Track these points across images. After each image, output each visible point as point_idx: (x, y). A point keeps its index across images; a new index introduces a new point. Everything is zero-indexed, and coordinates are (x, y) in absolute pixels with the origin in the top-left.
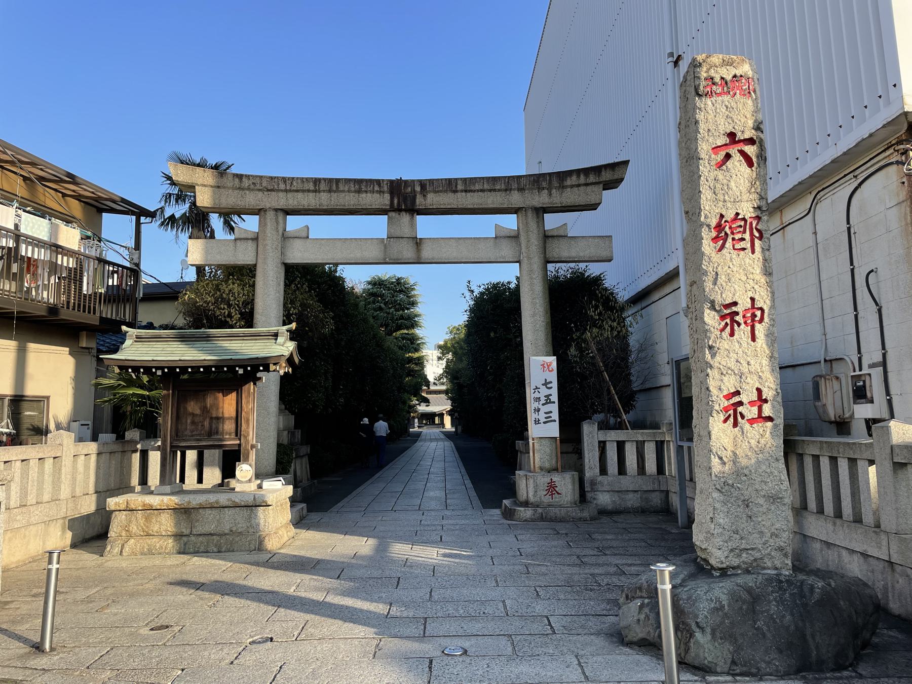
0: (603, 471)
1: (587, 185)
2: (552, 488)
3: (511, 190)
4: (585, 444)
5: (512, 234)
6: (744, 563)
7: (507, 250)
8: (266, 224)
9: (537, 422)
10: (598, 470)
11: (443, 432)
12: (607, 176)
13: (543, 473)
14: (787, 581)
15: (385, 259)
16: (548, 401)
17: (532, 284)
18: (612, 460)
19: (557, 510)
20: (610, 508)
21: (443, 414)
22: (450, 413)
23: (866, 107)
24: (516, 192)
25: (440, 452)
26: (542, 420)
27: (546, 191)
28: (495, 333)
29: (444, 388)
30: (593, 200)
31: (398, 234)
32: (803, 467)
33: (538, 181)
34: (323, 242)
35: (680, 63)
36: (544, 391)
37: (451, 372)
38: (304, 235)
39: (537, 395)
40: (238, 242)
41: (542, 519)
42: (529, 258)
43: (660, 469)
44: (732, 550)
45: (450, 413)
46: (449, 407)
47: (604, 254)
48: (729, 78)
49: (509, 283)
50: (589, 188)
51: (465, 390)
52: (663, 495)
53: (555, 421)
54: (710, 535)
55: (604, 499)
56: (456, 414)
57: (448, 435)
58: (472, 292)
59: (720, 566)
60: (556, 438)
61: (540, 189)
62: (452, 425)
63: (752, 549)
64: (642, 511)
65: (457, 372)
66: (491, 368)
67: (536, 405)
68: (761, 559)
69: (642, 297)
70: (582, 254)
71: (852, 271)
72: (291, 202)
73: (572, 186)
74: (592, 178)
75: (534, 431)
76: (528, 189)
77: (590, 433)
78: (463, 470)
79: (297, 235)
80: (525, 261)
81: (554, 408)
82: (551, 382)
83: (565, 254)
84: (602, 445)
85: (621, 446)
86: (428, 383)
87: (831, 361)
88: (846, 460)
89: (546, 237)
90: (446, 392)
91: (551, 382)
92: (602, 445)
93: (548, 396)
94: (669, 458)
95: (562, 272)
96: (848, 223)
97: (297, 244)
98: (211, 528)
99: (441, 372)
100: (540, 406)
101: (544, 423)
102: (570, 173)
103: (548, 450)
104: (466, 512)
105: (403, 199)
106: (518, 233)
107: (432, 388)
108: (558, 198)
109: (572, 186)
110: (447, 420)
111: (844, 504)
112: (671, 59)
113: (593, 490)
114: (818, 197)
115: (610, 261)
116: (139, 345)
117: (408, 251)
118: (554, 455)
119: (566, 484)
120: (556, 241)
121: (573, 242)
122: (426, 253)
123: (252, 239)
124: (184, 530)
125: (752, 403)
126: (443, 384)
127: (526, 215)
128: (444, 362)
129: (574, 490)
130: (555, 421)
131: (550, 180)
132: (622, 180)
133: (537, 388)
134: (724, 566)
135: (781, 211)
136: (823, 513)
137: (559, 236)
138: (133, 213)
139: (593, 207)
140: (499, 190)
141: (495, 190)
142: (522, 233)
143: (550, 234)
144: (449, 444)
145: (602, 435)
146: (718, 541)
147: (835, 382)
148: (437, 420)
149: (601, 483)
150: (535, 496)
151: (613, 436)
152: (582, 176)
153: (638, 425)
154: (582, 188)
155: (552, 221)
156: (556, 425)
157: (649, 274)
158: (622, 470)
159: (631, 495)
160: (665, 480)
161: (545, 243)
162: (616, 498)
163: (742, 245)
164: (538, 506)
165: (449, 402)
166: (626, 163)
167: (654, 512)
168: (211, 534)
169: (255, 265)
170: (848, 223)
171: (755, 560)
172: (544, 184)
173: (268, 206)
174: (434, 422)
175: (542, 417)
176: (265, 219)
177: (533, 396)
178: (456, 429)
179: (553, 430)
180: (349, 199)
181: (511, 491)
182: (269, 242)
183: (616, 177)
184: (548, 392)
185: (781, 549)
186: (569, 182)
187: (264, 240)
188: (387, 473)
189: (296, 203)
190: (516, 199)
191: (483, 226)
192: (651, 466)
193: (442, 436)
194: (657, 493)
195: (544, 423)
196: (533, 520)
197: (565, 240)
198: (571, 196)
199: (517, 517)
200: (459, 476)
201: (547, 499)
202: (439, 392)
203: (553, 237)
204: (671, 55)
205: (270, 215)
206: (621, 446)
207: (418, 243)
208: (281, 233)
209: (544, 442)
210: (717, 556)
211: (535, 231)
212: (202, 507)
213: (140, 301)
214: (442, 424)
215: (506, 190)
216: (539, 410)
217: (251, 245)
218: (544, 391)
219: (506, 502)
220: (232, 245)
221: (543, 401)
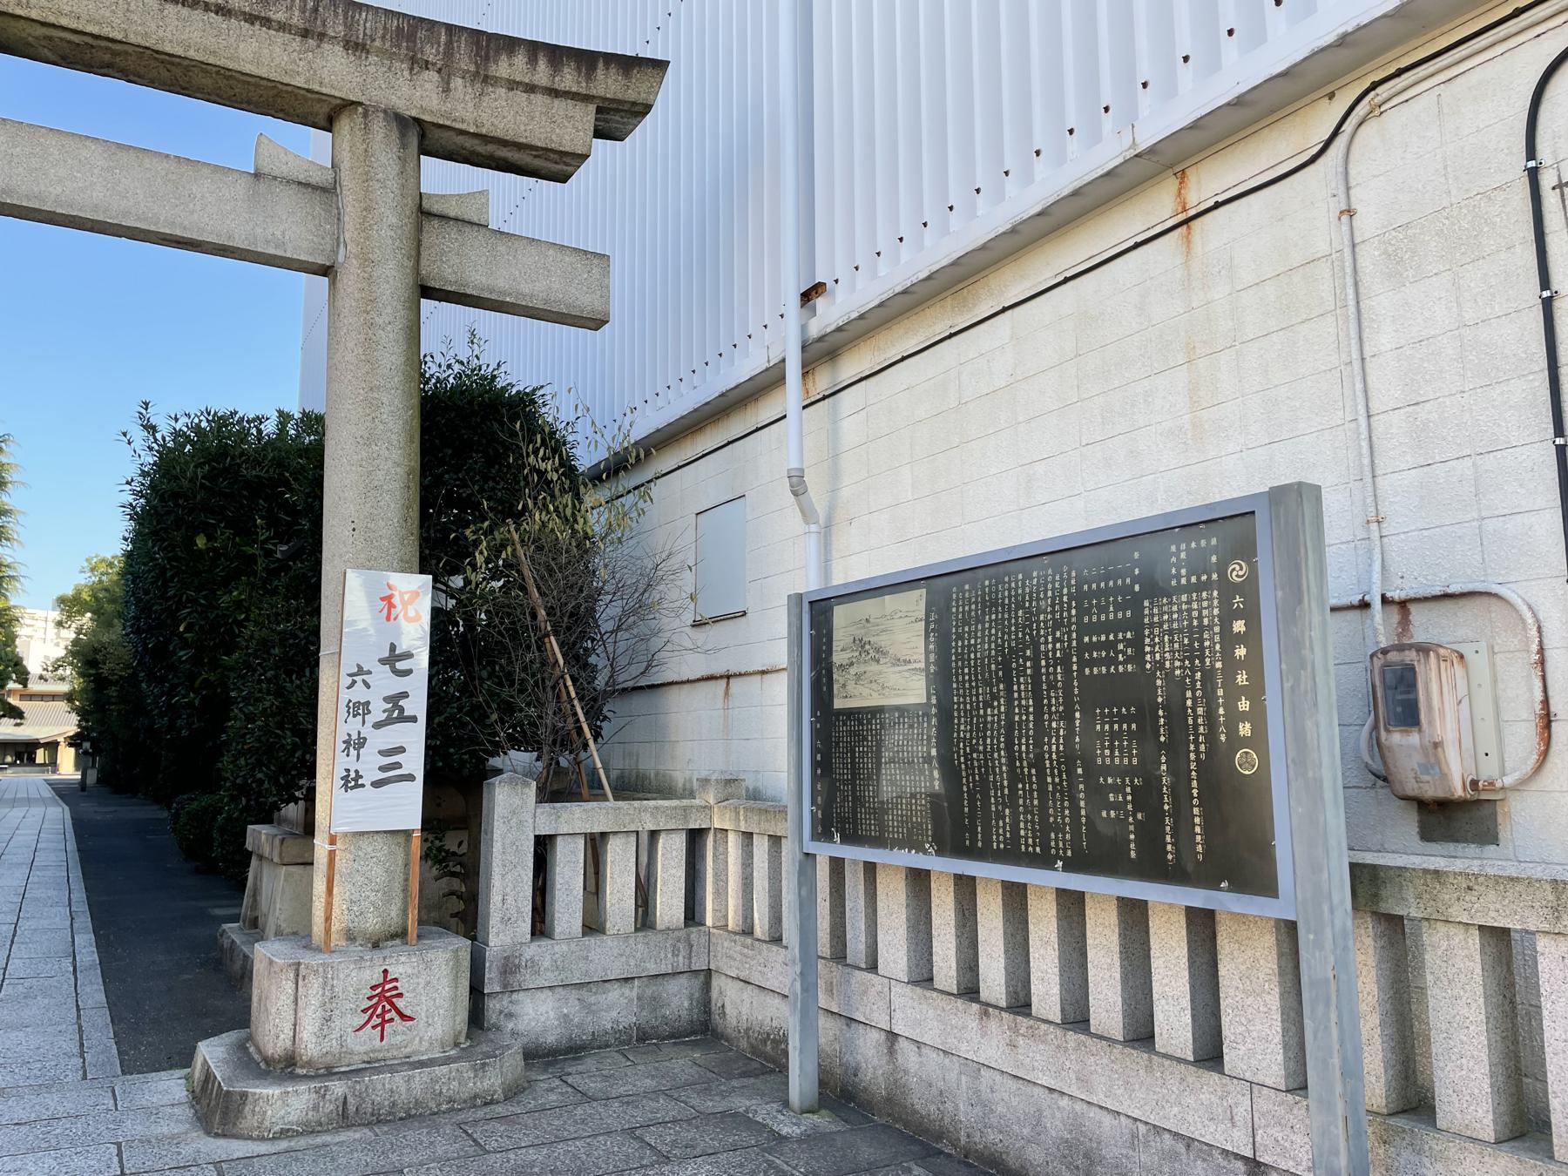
0: (541, 924)
1: (554, 93)
2: (384, 1003)
3: (322, 36)
4: (497, 847)
5: (316, 178)
9: (352, 781)
10: (526, 926)
11: (51, 783)
12: (608, 84)
13: (356, 948)
16: (396, 714)
18: (569, 890)
19: (398, 1081)
20: (551, 1039)
21: (58, 744)
22: (74, 742)
23: (951, 208)
24: (339, 49)
25: (26, 836)
26: (370, 774)
27: (432, 75)
28: (210, 538)
29: (64, 688)
32: (1297, 952)
33: (411, 37)
36: (384, 683)
37: (87, 657)
39: (359, 694)
41: (345, 1118)
42: (366, 261)
43: (692, 913)
45: (74, 742)
46: (71, 727)
47: (585, 302)
49: (260, 420)
50: (560, 105)
51: (113, 692)
52: (697, 983)
53: (410, 778)
55: (536, 1014)
56: (87, 745)
57: (63, 792)
58: (151, 429)
60: (407, 834)
61: (417, 63)
62: (77, 766)
64: (643, 1039)
65: (96, 651)
66: (189, 629)
67: (354, 726)
69: (617, 466)
70: (525, 288)
71: (1548, 305)
73: (513, 85)
74: (568, 79)
75: (337, 809)
76: (381, 52)
77: (513, 810)
78: (79, 894)
80: (350, 279)
81: (413, 740)
82: (408, 655)
84: (543, 847)
85: (596, 844)
86: (23, 677)
87: (1403, 605)
88: (1475, 939)
89: (424, 214)
90: (69, 697)
91: (408, 655)
92: (543, 847)
93: (395, 700)
94: (721, 877)
95: (434, 369)
96: (1531, 153)
99: (62, 653)
100: (367, 731)
101: (377, 784)
102: (511, 44)
103: (378, 874)
104: (52, 1101)
107: (35, 686)
109: (513, 85)
110: (67, 756)
111: (680, 873)
113: (508, 989)
114: (1361, 110)
118: (397, 886)
119: (431, 979)
120: (452, 231)
121: (502, 249)
126: (62, 679)
128: (69, 634)
129: (454, 999)
130: (410, 778)
131: (449, 43)
132: (646, 109)
133: (360, 671)
135: (1182, 175)
136: (1085, 1022)
140: (282, 27)
141: (267, 22)
143: (436, 208)
144: (59, 814)
145: (549, 819)
147: (1458, 669)
148: (40, 757)
149: (533, 964)
150: (322, 1035)
151: (575, 819)
152: (542, 64)
153: (631, 787)
154: (539, 99)
156: (414, 793)
157: (660, 401)
158: (593, 925)
159: (615, 994)
160: (703, 940)
161: (419, 229)
162: (572, 1007)
164: (330, 1073)
165: (75, 718)
166: (661, 65)
167: (672, 1036)
170: (1531, 153)
172: (430, 53)
174: (32, 761)
175: (369, 764)
177: (345, 695)
178: (84, 775)
179: (405, 807)
181: (225, 996)
183: (631, 95)
184: (398, 685)
186: (503, 68)
192: (669, 903)
193: (47, 793)
194: (683, 980)
195: (377, 784)
196: (309, 1130)
199: (249, 1121)
200: (60, 918)
201: (365, 1043)
202: (54, 697)
203: (444, 218)
206: (596, 844)
209: (367, 846)
211: (393, 184)
213: (25, 686)
214: (53, 763)
215: (305, 34)
216: (361, 743)
218: (384, 683)
221: (378, 714)
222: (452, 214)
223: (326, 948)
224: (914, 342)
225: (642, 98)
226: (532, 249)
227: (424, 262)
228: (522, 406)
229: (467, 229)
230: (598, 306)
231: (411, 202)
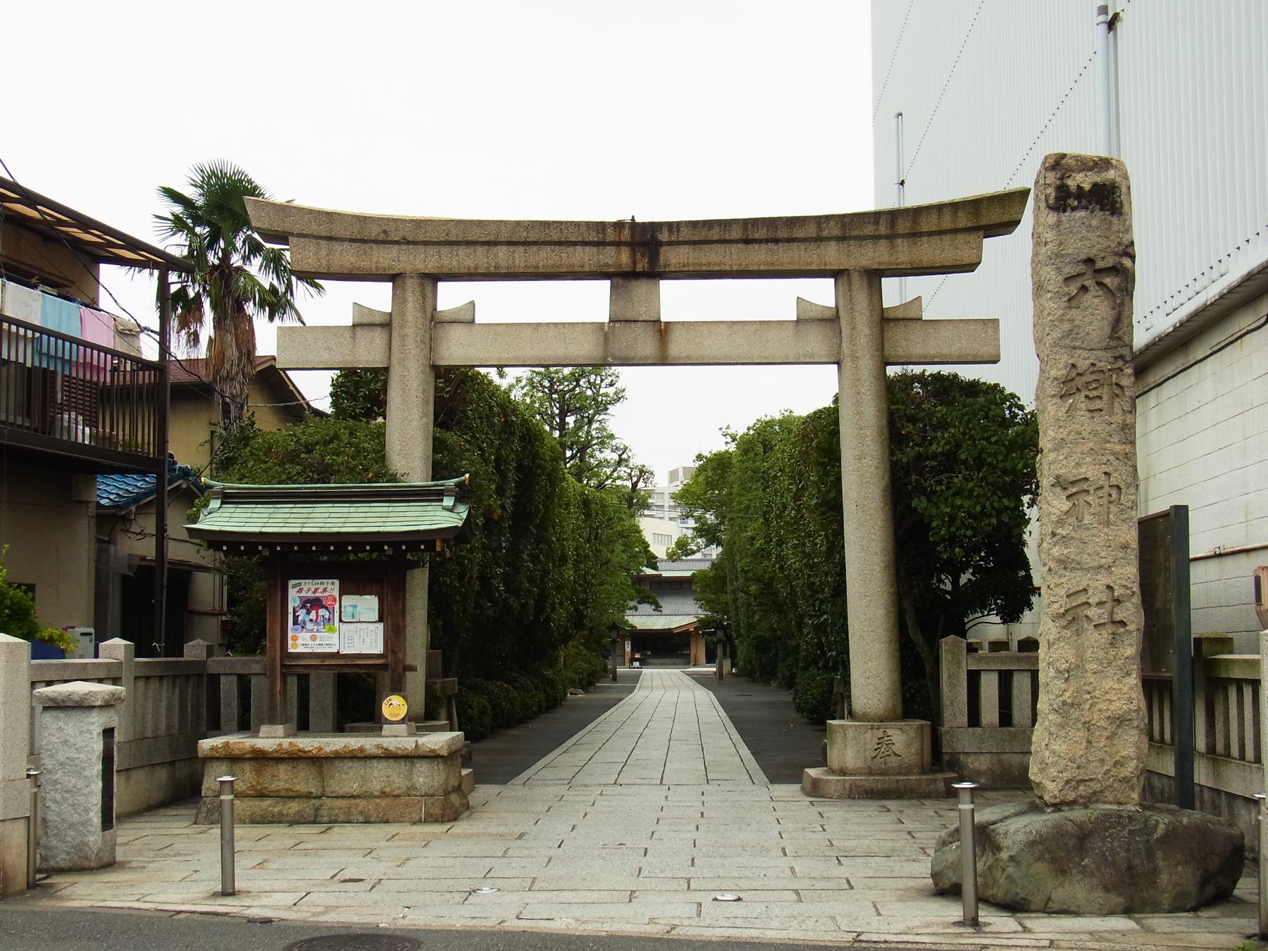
0: (974, 718)
5: (827, 315)
6: (1081, 796)
7: (816, 341)
8: (405, 301)
14: (1129, 817)
15: (605, 358)
17: (858, 403)
18: (229, 705)
30: (966, 256)
31: (630, 314)
34: (500, 329)
35: (1118, 25)
38: (468, 317)
40: (359, 331)
42: (855, 358)
43: (974, 678)
44: (1067, 782)
47: (985, 351)
48: (1087, 187)
50: (960, 237)
54: (1044, 766)
59: (1053, 801)
63: (1091, 780)
68: (1101, 791)
70: (945, 351)
72: (446, 262)
79: (454, 317)
80: (847, 363)
83: (918, 351)
89: (885, 321)
97: (456, 332)
98: (354, 787)
105: (639, 254)
106: (838, 316)
108: (904, 253)
112: (1102, 18)
115: (995, 362)
116: (229, 508)
117: (646, 344)
121: (931, 330)
122: (677, 346)
123: (382, 325)
124: (313, 790)
125: (1100, 604)
127: (850, 285)
132: (1018, 222)
134: (1058, 800)
137: (908, 318)
138: (155, 265)
139: (970, 267)
142: (842, 314)
143: (891, 315)
146: (1053, 771)
155: (894, 292)
163: (1098, 404)
168: (353, 797)
169: (386, 369)
171: (1095, 793)
173: (409, 268)
176: (404, 290)
180: (545, 257)
182: (410, 331)
185: (1125, 780)
187: (402, 327)
188: (563, 759)
189: (455, 263)
190: (832, 254)
191: (775, 300)
197: (917, 326)
198: (929, 251)
203: (896, 320)
204: (1103, 10)
205: (411, 285)
207: (663, 331)
208: (429, 315)
210: (1051, 789)
211: (866, 312)
212: (338, 757)
217: (379, 337)
219: (813, 772)
220: (347, 335)
222: (901, 316)
223: (449, 698)
224: (179, 896)
225: (1014, 217)
226: (950, 327)
227: (887, 348)
228: (995, 388)
229: (910, 323)
230: (992, 351)
231: (876, 318)
